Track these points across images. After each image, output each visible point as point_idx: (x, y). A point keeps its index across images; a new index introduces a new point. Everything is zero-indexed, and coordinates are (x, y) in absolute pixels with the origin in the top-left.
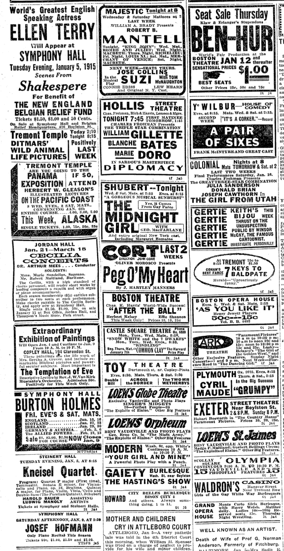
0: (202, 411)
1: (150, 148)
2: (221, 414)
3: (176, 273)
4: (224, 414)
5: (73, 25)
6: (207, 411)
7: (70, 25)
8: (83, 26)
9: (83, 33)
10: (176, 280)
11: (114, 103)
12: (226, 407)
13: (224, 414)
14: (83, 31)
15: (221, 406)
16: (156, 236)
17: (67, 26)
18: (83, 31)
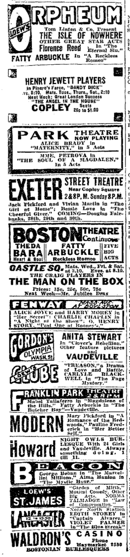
0: (22, 192)
1: (21, 256)
2: (44, 431)
3: (40, 447)
4: (48, 431)
5: (48, 417)
6: (29, 194)
7: (46, 417)
8: (43, 535)
9: (57, 192)
10: (39, 454)
11: (49, 533)
12: (57, 185)
13: (48, 431)
14: (58, 189)
15: (50, 184)
16: (89, 420)
17: (42, 419)
18: (58, 189)
